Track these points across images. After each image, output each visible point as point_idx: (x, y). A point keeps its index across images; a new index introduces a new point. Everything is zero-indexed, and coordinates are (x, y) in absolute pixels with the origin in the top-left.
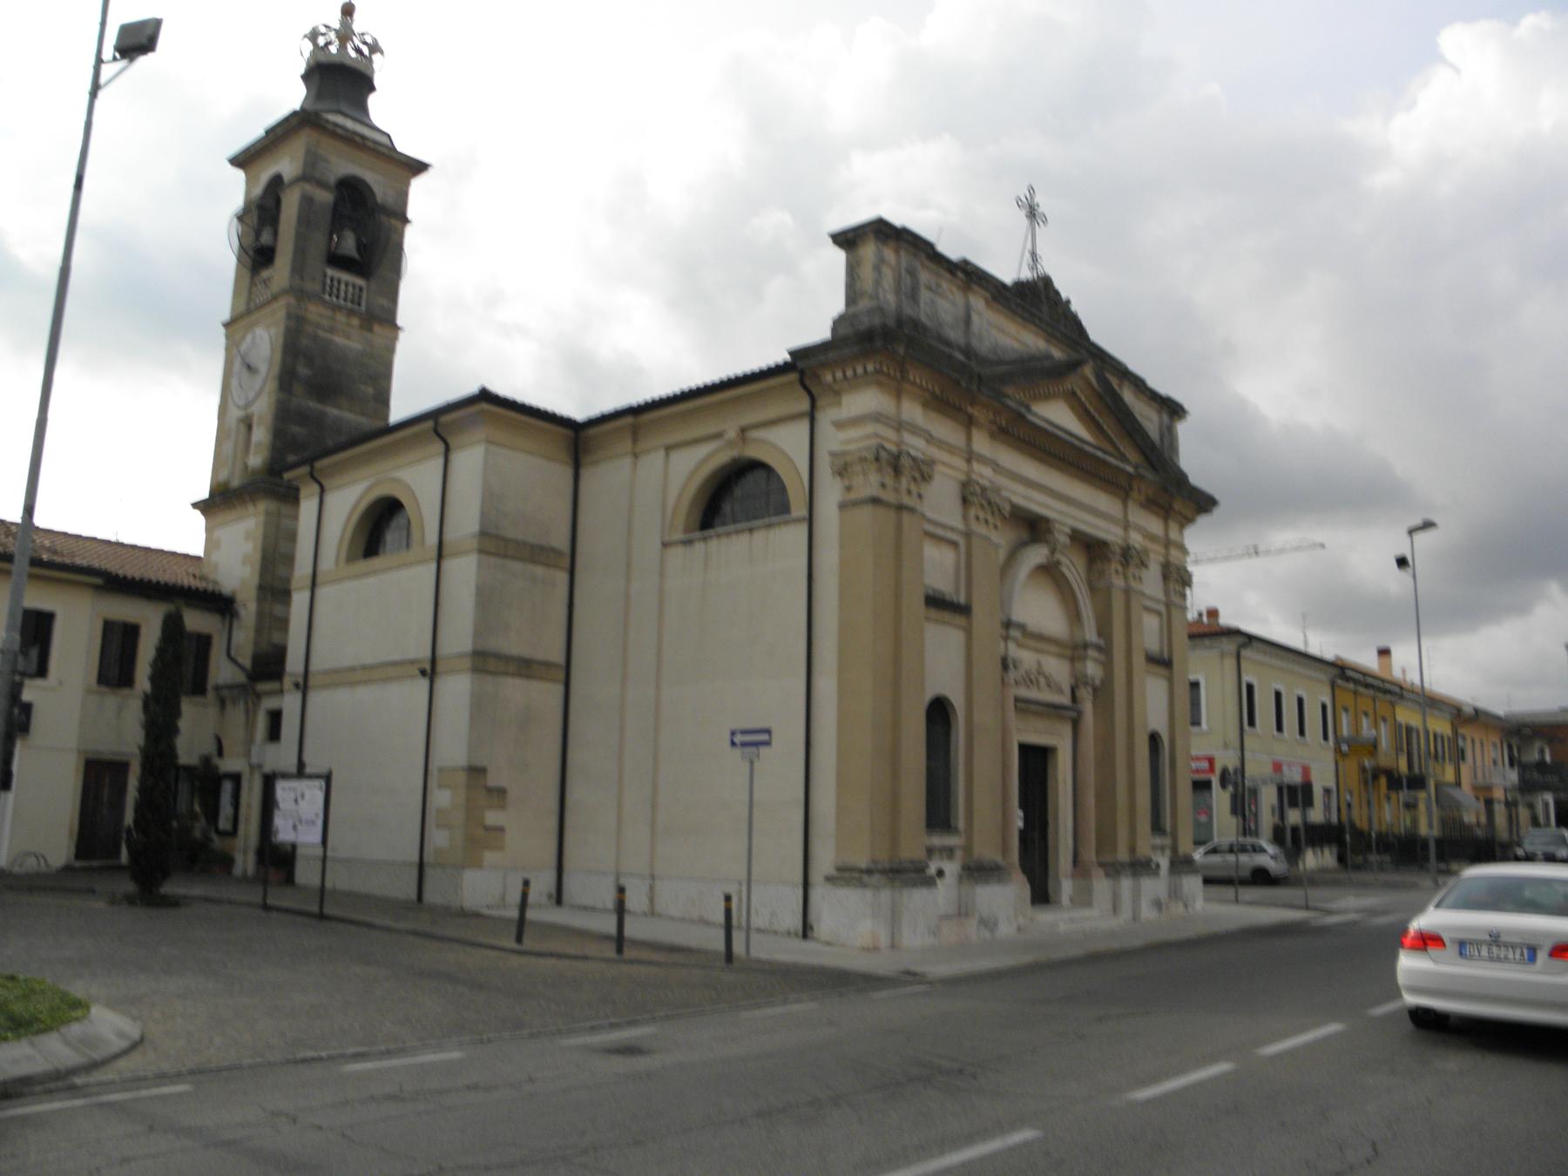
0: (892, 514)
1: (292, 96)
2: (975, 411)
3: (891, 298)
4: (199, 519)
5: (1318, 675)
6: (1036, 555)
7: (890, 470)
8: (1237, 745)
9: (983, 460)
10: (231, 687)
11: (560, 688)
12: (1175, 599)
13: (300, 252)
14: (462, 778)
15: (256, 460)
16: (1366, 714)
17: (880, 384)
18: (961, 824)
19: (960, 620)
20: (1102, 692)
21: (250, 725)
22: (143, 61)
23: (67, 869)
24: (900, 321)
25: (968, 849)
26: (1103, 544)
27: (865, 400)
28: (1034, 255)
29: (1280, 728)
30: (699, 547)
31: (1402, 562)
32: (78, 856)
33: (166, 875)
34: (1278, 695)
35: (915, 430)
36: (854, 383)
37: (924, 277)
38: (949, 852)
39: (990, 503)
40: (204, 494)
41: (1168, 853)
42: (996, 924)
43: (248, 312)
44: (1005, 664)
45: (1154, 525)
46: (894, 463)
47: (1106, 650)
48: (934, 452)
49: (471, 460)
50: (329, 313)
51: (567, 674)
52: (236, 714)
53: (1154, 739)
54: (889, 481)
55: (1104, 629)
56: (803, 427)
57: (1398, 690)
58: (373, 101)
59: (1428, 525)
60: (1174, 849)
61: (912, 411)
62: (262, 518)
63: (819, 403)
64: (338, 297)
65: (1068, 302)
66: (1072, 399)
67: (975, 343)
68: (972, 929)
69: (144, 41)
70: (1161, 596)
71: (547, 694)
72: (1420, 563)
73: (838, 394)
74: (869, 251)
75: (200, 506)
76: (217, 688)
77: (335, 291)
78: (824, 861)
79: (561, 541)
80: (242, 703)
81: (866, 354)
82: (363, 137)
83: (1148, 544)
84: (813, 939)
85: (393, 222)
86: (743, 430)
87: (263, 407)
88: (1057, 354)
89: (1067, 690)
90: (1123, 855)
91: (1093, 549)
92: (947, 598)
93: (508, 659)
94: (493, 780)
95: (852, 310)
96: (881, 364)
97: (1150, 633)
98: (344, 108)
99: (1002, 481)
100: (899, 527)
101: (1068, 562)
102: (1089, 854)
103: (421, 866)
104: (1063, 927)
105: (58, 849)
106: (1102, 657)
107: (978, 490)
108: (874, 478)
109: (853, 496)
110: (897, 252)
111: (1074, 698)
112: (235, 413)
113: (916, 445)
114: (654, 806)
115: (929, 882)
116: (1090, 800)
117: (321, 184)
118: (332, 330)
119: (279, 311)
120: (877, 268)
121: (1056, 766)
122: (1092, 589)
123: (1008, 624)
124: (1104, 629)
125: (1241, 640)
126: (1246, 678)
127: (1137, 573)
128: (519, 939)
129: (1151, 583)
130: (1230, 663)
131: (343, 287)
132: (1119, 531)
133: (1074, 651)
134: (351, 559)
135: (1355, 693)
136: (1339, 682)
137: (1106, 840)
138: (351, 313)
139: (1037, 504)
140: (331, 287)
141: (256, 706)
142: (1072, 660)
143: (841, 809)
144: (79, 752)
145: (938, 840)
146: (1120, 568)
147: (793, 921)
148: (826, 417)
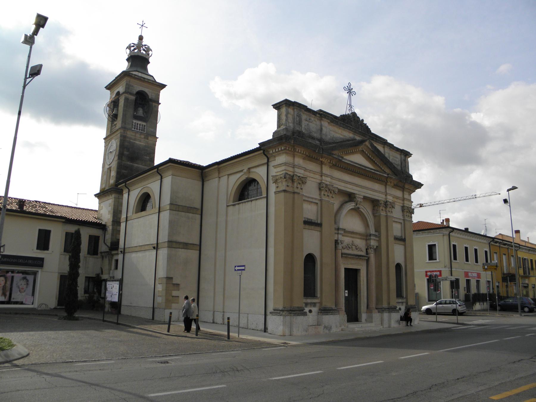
0: (292, 195)
1: (124, 66)
2: (323, 160)
3: (291, 125)
4: (97, 200)
5: (485, 241)
6: (351, 205)
7: (290, 181)
8: (449, 267)
9: (327, 176)
10: (104, 252)
11: (198, 252)
12: (406, 218)
13: (124, 115)
14: (165, 280)
15: (112, 181)
16: (505, 254)
17: (286, 153)
18: (319, 295)
19: (318, 228)
20: (377, 250)
21: (110, 264)
22: (37, 78)
23: (55, 308)
24: (294, 133)
25: (321, 303)
26: (378, 201)
27: (282, 159)
28: (350, 105)
29: (467, 260)
30: (237, 206)
31: (505, 201)
32: (58, 305)
33: (75, 311)
34: (466, 249)
35: (299, 167)
36: (279, 153)
37: (304, 116)
38: (314, 304)
39: (329, 190)
40: (98, 191)
41: (404, 304)
42: (331, 328)
43: (110, 135)
44: (336, 242)
45: (398, 193)
46: (291, 178)
47: (379, 237)
48: (307, 174)
49: (168, 180)
50: (134, 134)
51: (200, 247)
52: (106, 261)
53: (398, 266)
54: (290, 184)
55: (378, 229)
56: (265, 167)
57: (518, 245)
58: (149, 67)
59: (514, 188)
60: (407, 303)
61: (299, 161)
62: (113, 199)
63: (270, 160)
64: (137, 129)
65: (363, 120)
66: (363, 153)
67: (324, 137)
68: (321, 329)
69: (36, 72)
70: (402, 218)
71: (193, 254)
72: (512, 201)
73: (275, 157)
74: (284, 110)
75: (96, 195)
76: (101, 253)
77: (136, 127)
78: (270, 308)
79: (198, 206)
80: (108, 258)
81: (281, 144)
82: (144, 78)
83: (395, 200)
84: (267, 332)
85: (154, 104)
86: (249, 169)
87: (114, 165)
88: (358, 138)
89: (365, 251)
90: (385, 305)
91: (375, 203)
92: (313, 221)
93: (180, 243)
94: (175, 282)
95: (279, 129)
96: (286, 147)
97: (396, 230)
98: (139, 70)
99: (334, 181)
100: (294, 198)
101: (363, 207)
102: (373, 305)
103: (153, 308)
104: (357, 329)
105: (52, 303)
106: (378, 239)
107: (324, 186)
108: (284, 183)
109: (278, 190)
110: (293, 109)
111: (367, 253)
112: (107, 167)
113: (300, 172)
114: (224, 290)
115: (305, 314)
116: (373, 286)
117: (131, 94)
118: (135, 140)
119: (118, 134)
120: (287, 116)
121: (360, 276)
122: (375, 216)
123: (338, 229)
124: (378, 229)
125: (450, 229)
126: (452, 243)
127: (390, 210)
128: (168, 331)
129: (397, 213)
130: (446, 238)
131: (139, 126)
132: (384, 196)
133: (367, 237)
134: (137, 212)
135: (500, 247)
136: (492, 243)
137: (379, 300)
138: (141, 134)
139: (350, 189)
140: (135, 126)
141: (112, 258)
142: (366, 240)
143: (275, 290)
144: (59, 273)
145: (309, 301)
146: (384, 209)
147: (262, 327)
148: (272, 164)
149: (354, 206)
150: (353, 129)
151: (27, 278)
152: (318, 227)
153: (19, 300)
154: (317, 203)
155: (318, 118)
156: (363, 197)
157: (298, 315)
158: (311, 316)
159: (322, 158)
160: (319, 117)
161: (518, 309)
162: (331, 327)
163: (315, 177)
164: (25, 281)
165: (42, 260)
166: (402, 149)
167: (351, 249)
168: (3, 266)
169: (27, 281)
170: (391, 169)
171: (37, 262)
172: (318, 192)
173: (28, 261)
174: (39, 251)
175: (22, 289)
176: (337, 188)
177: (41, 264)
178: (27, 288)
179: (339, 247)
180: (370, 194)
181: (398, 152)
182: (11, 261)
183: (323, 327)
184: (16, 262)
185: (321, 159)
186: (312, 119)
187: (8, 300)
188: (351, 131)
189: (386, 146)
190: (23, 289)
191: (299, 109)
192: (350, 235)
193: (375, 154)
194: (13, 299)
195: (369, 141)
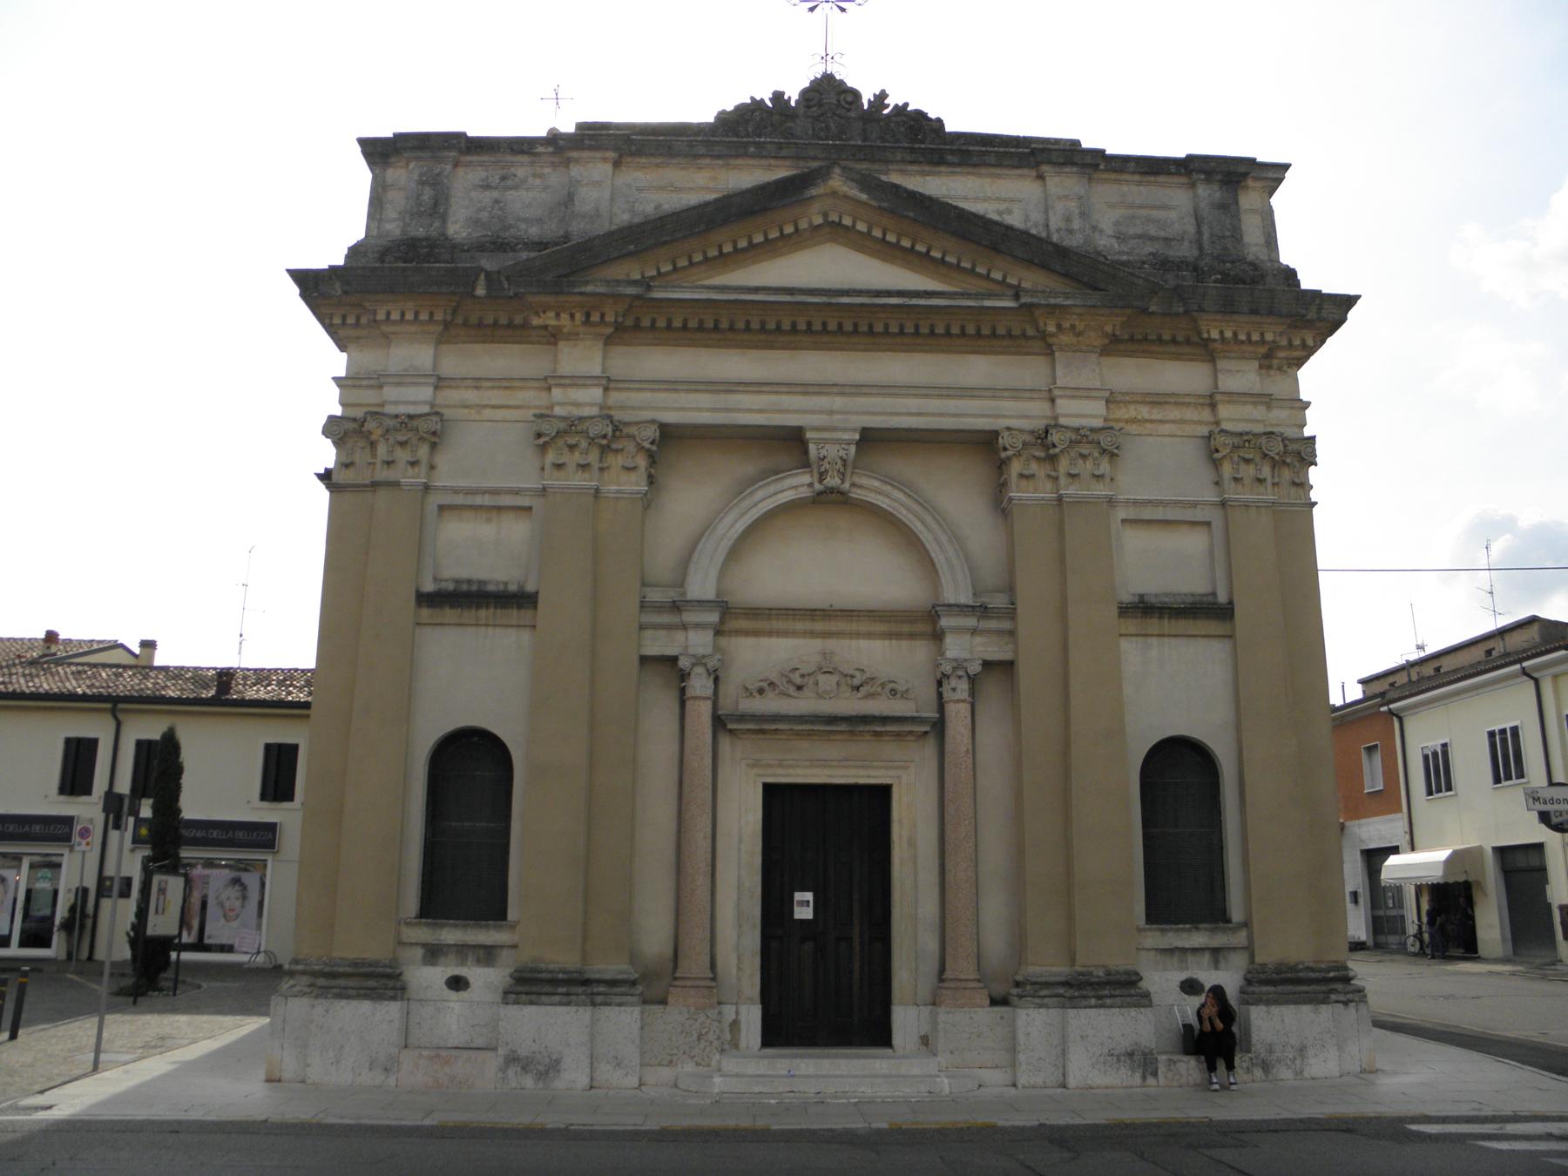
38: (487, 955)
70: (1210, 495)
149: (811, 485)
150: (780, 146)
151: (243, 880)
152: (523, 611)
153: (224, 940)
154: (1208, 524)
155: (552, 159)
156: (857, 437)
157: (339, 996)
158: (457, 1006)
159: (537, 314)
160: (552, 154)
161: (101, 974)
162: (558, 1062)
163: (511, 403)
164: (237, 888)
165: (271, 828)
166: (1182, 154)
167: (806, 692)
168: (17, 845)
169: (244, 888)
170: (1043, 266)
171: (258, 835)
172: (1206, 474)
173: (30, 827)
174: (266, 804)
175: (230, 910)
176: (653, 421)
177: (66, 833)
178: (243, 906)
179: (693, 687)
180: (910, 414)
181: (1161, 179)
182: (193, 834)
183: (501, 1060)
184: (26, 832)
185: (536, 321)
186: (521, 172)
187: (196, 941)
188: (772, 162)
189: (1045, 168)
190: (234, 910)
191: (430, 154)
192: (800, 626)
193: (907, 217)
194: (209, 937)
195: (844, 168)
